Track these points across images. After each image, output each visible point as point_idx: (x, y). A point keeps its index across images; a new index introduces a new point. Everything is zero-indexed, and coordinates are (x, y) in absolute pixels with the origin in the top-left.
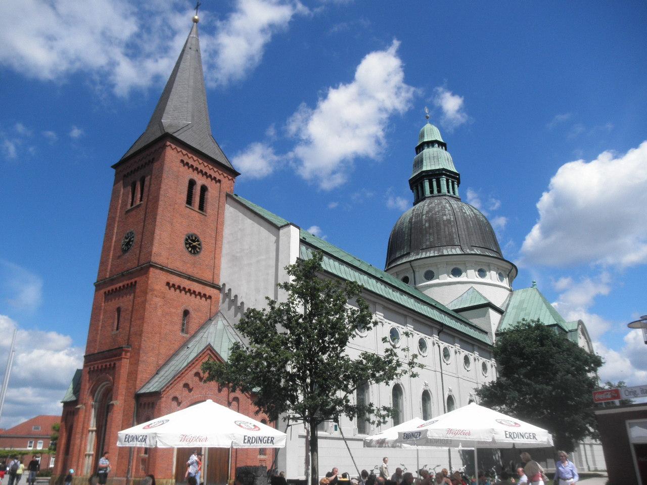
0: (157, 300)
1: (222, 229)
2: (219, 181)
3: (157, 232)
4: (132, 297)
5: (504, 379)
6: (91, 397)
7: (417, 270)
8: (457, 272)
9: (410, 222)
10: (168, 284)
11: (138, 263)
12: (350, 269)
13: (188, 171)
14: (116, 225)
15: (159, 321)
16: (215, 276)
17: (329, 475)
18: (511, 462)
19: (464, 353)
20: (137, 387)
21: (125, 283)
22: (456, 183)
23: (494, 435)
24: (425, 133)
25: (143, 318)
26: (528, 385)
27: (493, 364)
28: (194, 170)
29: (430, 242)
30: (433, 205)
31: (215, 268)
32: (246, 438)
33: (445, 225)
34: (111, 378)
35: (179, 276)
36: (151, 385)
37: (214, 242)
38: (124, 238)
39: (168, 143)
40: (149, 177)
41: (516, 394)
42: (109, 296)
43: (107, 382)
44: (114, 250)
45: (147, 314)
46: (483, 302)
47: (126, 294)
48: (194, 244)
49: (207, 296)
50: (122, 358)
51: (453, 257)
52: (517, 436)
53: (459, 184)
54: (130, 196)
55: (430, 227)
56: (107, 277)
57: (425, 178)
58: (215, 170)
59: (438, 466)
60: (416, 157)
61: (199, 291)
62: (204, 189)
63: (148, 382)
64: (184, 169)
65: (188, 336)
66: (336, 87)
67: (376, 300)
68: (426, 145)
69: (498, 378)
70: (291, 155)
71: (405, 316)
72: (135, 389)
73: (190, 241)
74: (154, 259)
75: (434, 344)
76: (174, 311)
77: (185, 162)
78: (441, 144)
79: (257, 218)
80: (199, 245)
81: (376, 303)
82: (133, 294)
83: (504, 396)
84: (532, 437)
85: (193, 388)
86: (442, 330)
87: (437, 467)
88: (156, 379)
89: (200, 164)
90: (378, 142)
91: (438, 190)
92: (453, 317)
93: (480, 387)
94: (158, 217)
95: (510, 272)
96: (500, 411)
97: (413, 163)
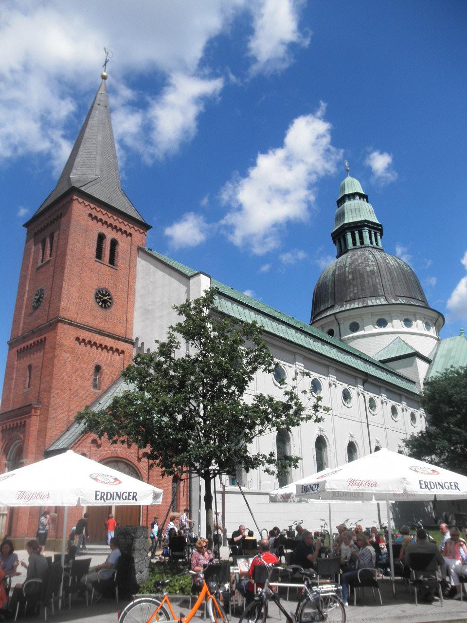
0: (67, 356)
1: (135, 283)
2: (130, 235)
3: (65, 287)
4: (42, 353)
5: (433, 428)
6: (4, 456)
7: (341, 322)
8: (382, 323)
9: (334, 275)
10: (77, 339)
11: (48, 319)
12: (267, 319)
13: (97, 225)
14: (28, 283)
15: (69, 377)
16: (128, 330)
17: (236, 534)
18: (444, 514)
19: (369, 395)
20: (47, 445)
21: (36, 339)
22: (378, 234)
23: (405, 485)
24: (346, 186)
25: (52, 375)
26: (458, 433)
27: (422, 414)
28: (103, 224)
29: (355, 294)
30: (356, 257)
31: (127, 322)
32: (98, 493)
33: (368, 276)
34: (22, 436)
35: (89, 330)
36: (60, 442)
37: (126, 296)
38: (34, 296)
39: (75, 197)
40: (58, 232)
41: (446, 443)
42: (22, 353)
43: (19, 441)
44: (26, 307)
45: (55, 371)
46: (409, 351)
47: (36, 351)
48: (105, 298)
49: (120, 351)
50: (31, 415)
51: (378, 307)
52: (435, 485)
53: (381, 235)
54: (41, 253)
55: (353, 279)
56: (20, 335)
57: (347, 231)
58: (126, 223)
59: (360, 521)
60: (338, 210)
61: (111, 346)
62: (114, 243)
63: (58, 439)
64: (92, 223)
65: (100, 391)
66: (265, 152)
67: (296, 350)
68: (347, 198)
69: (426, 428)
70: (223, 222)
71: (327, 366)
72: (45, 446)
73: (100, 296)
74: (63, 314)
75: (359, 394)
76: (85, 366)
77: (93, 216)
78: (362, 196)
79: (168, 269)
80: (110, 299)
81: (295, 353)
82: (43, 351)
83: (434, 445)
84: (453, 487)
85: (101, 444)
86: (367, 380)
87: (359, 522)
88: (66, 436)
89: (136, 231)
90: (309, 208)
91: (360, 242)
92: (379, 366)
93: (408, 437)
94: (66, 272)
95: (436, 320)
96: (431, 462)
97: (335, 217)
